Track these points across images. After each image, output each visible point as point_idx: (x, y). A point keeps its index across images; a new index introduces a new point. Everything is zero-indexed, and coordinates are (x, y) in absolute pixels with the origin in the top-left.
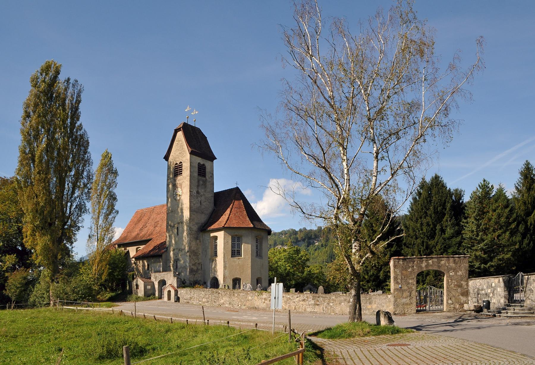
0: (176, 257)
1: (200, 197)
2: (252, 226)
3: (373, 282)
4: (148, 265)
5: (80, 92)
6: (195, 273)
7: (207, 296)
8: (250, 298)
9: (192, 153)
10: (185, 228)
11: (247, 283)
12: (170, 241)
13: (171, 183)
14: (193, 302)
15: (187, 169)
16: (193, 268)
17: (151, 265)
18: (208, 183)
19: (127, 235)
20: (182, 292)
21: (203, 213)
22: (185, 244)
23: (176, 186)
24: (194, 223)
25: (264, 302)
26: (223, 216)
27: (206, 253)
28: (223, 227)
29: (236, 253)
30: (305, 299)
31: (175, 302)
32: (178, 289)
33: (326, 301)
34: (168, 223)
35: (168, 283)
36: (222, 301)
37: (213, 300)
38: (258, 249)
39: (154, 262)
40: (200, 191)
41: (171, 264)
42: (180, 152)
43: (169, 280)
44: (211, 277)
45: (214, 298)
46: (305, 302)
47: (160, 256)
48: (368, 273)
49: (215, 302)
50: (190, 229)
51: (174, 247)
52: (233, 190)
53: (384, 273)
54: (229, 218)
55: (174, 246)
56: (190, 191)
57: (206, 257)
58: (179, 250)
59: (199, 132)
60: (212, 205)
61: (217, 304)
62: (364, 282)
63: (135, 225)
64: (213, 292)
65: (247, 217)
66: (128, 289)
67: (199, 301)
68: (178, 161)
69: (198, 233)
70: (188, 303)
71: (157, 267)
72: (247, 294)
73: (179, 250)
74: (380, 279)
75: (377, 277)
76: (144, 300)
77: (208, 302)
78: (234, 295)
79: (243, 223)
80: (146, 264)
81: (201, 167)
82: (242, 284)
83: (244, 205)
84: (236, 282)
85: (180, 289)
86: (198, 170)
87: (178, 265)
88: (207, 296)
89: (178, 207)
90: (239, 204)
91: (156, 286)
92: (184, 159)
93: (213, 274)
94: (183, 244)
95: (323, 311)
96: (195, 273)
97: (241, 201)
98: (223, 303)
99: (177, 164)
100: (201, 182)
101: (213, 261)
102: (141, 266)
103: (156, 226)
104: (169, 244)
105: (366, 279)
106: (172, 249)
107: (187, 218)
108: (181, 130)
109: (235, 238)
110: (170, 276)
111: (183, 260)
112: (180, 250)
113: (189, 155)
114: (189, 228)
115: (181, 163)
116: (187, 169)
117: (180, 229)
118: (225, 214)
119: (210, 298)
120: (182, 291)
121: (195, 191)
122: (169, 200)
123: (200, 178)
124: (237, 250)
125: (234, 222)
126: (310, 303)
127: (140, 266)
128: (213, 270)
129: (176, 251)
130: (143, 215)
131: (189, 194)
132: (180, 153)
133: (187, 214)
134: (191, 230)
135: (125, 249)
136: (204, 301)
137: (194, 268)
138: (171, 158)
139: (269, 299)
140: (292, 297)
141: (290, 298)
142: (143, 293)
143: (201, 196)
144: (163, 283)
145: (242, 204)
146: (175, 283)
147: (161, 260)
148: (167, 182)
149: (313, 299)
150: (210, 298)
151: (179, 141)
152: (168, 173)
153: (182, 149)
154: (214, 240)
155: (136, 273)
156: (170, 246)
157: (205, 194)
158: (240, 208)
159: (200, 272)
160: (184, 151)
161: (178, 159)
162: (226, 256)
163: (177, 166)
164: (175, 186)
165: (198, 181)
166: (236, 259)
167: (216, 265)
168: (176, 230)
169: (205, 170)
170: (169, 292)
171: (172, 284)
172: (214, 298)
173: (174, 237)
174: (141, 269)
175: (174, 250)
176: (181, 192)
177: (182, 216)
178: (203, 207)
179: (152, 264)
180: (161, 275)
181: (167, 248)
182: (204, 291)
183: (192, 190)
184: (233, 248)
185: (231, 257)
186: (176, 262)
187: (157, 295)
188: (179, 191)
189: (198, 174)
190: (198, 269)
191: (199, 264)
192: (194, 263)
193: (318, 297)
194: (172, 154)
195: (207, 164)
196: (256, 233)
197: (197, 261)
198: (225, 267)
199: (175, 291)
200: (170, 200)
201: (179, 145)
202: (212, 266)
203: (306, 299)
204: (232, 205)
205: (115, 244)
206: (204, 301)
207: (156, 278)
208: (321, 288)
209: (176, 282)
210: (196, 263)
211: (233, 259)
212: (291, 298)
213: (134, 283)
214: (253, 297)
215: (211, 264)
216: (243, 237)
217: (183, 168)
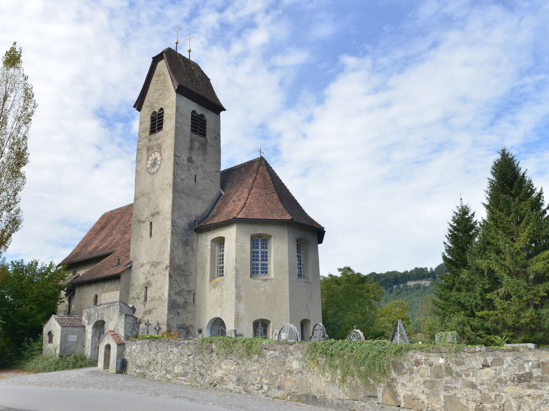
1: (193, 169)
7: (185, 359)
8: (295, 365)
14: (153, 373)
16: (176, 300)
17: (101, 296)
18: (209, 149)
19: (81, 251)
21: (199, 197)
24: (182, 214)
29: (260, 270)
31: (118, 372)
32: (126, 342)
35: (110, 326)
36: (219, 374)
37: (198, 369)
38: (301, 264)
40: (194, 158)
42: (161, 92)
45: (200, 363)
46: (534, 387)
47: (116, 278)
49: (201, 375)
52: (254, 162)
54: (245, 203)
56: (175, 155)
59: (197, 69)
61: (207, 380)
63: (96, 235)
67: (167, 371)
68: (157, 107)
69: (189, 233)
72: (286, 353)
77: (185, 374)
81: (197, 118)
82: (273, 332)
85: (129, 342)
86: (192, 123)
88: (185, 359)
92: (166, 102)
98: (222, 380)
100: (197, 144)
108: (163, 58)
109: (258, 240)
113: (175, 94)
119: (191, 364)
120: (134, 347)
121: (185, 157)
123: (195, 136)
124: (258, 260)
130: (110, 219)
131: (172, 160)
132: (160, 95)
135: (74, 274)
136: (176, 371)
137: (178, 299)
143: (197, 168)
146: (121, 327)
153: (165, 87)
157: (203, 164)
161: (156, 105)
165: (192, 141)
166: (258, 281)
169: (205, 125)
171: (116, 331)
172: (200, 363)
182: (177, 346)
183: (177, 154)
184: (253, 260)
185: (251, 277)
189: (192, 130)
190: (186, 302)
192: (179, 290)
194: (148, 98)
195: (209, 116)
201: (160, 82)
206: (176, 371)
210: (182, 290)
216: (272, 238)
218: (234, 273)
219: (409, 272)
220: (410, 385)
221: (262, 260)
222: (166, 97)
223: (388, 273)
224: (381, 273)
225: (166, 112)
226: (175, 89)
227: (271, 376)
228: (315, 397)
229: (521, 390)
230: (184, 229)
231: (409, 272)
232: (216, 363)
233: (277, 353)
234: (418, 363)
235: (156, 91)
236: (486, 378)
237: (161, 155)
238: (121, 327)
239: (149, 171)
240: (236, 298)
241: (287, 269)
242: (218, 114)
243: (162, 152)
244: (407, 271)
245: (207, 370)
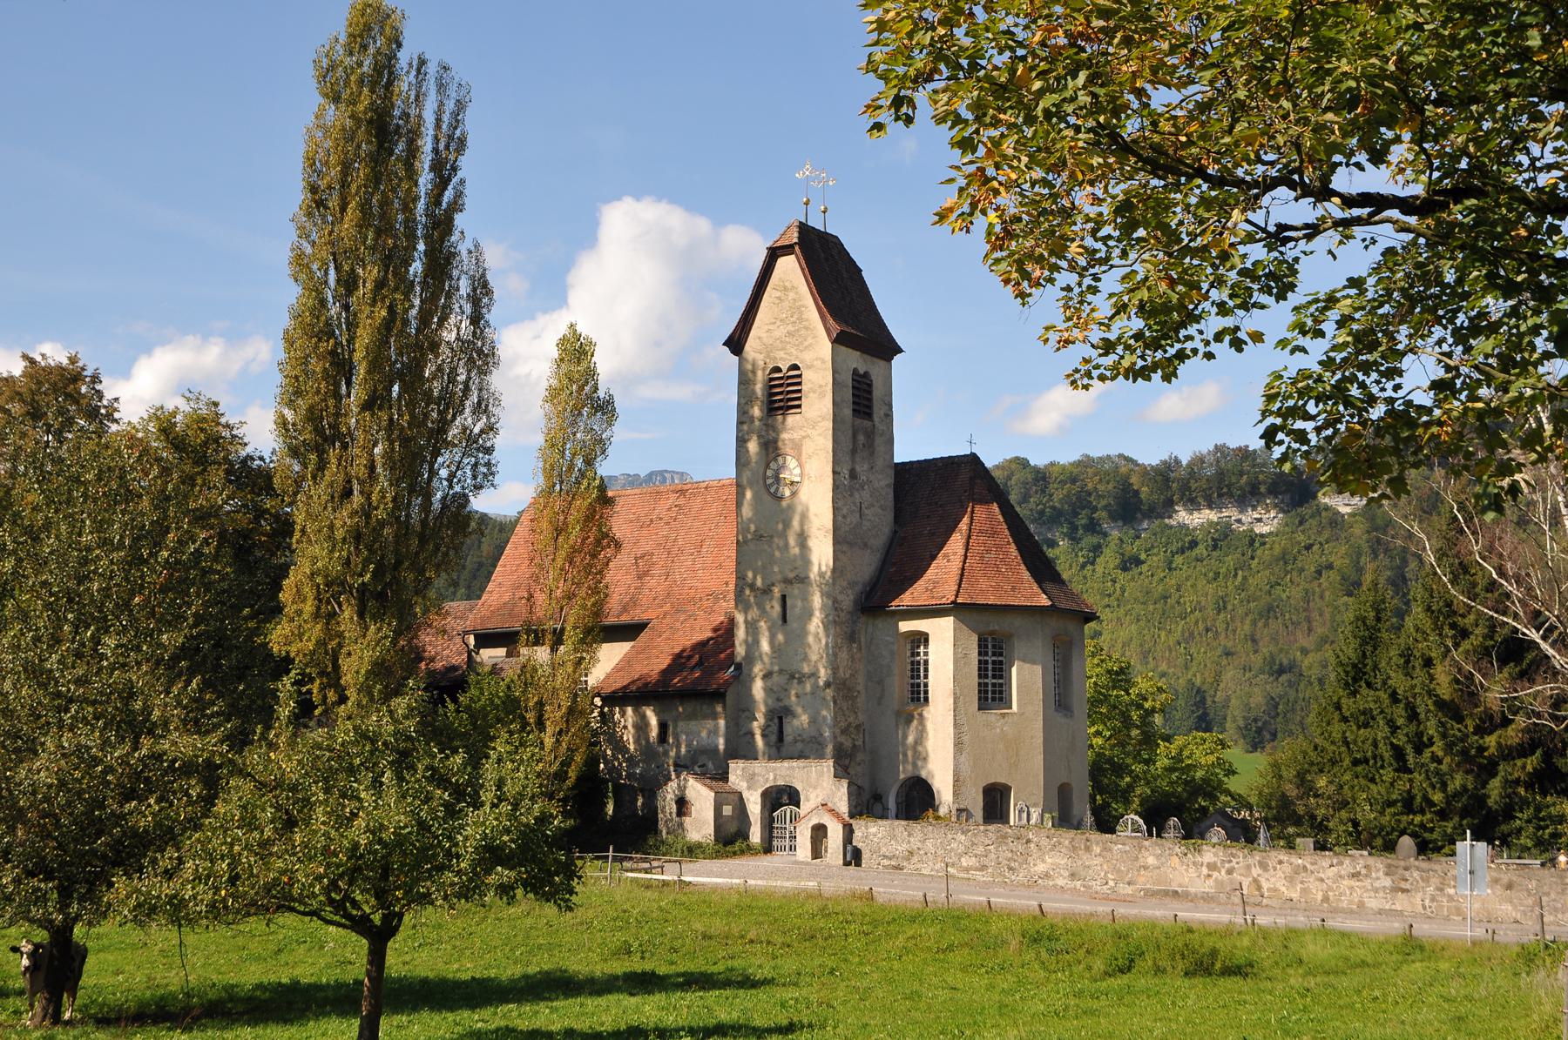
0: (779, 700)
2: (1044, 601)
3: (1462, 818)
4: (663, 727)
5: (461, 106)
6: (847, 762)
8: (1151, 860)
9: (839, 340)
10: (817, 601)
11: (1027, 805)
12: (752, 645)
13: (755, 438)
15: (823, 395)
17: (675, 727)
20: (871, 833)
22: (814, 657)
23: (777, 448)
24: (845, 584)
25: (1209, 876)
26: (939, 561)
27: (883, 690)
28: (952, 603)
30: (1359, 873)
32: (851, 821)
33: (1433, 880)
34: (741, 578)
36: (1041, 868)
39: (691, 717)
40: (858, 468)
41: (757, 727)
42: (790, 328)
43: (815, 788)
44: (902, 776)
45: (1010, 855)
47: (718, 696)
48: (1444, 785)
49: (1010, 869)
50: (834, 605)
51: (768, 666)
53: (1504, 788)
54: (963, 569)
55: (766, 659)
56: (834, 472)
57: (879, 703)
58: (787, 674)
60: (890, 516)
62: (1429, 816)
64: (1005, 837)
65: (1023, 567)
66: (610, 812)
68: (781, 359)
70: (898, 868)
71: (704, 734)
73: (792, 677)
74: (1490, 808)
75: (1481, 800)
76: (718, 855)
77: (983, 868)
78: (1088, 849)
79: (1013, 589)
80: (653, 721)
83: (1006, 522)
84: (995, 803)
85: (862, 822)
87: (787, 730)
89: (787, 524)
90: (991, 518)
91: (754, 807)
93: (910, 768)
94: (806, 658)
95: (1424, 908)
96: (847, 762)
97: (995, 507)
99: (778, 370)
100: (861, 438)
101: (909, 721)
102: (630, 728)
103: (646, 573)
104: (747, 652)
105: (1435, 805)
106: (758, 669)
107: (824, 568)
110: (820, 775)
111: (805, 710)
112: (795, 677)
113: (829, 345)
114: (830, 602)
115: (795, 367)
116: (823, 395)
117: (795, 605)
118: (946, 556)
119: (993, 856)
122: (744, 495)
123: (858, 421)
125: (984, 584)
126: (1377, 884)
127: (625, 727)
128: (910, 753)
129: (775, 678)
131: (829, 481)
132: (790, 334)
133: (822, 553)
134: (836, 609)
136: (965, 864)
138: (752, 346)
139: (1227, 865)
140: (1312, 864)
141: (1305, 867)
142: (711, 830)
144: (781, 798)
145: (1000, 517)
146: (841, 800)
147: (719, 709)
148: (738, 430)
149: (1387, 874)
150: (993, 856)
151: (785, 289)
152: (743, 401)
154: (909, 647)
155: (609, 752)
156: (750, 658)
158: (994, 534)
159: (860, 757)
160: (807, 328)
161: (781, 354)
162: (960, 704)
163: (781, 378)
164: (771, 449)
167: (922, 732)
168: (778, 608)
170: (819, 832)
172: (1010, 855)
173: (770, 629)
174: (629, 737)
175: (767, 676)
176: (797, 471)
177: (807, 562)
178: (866, 525)
179: (681, 724)
180: (774, 770)
181: (739, 667)
186: (776, 721)
187: (756, 836)
188: (792, 471)
189: (854, 410)
190: (854, 746)
191: (858, 727)
193: (1406, 869)
195: (874, 368)
196: (1055, 624)
197: (851, 719)
198: (958, 745)
199: (844, 826)
200: (749, 495)
201: (786, 304)
202: (905, 737)
203: (1364, 871)
204: (966, 519)
205: (467, 633)
207: (751, 779)
208: (1406, 842)
209: (845, 798)
211: (985, 716)
212: (1309, 866)
213: (670, 792)
214: (1163, 860)
215: (900, 733)
217: (804, 387)
218: (952, 701)
219: (1184, 463)
220: (1273, 880)
221: (994, 677)
222: (806, 343)
223: (1086, 463)
224: (1052, 464)
225: (808, 376)
226: (829, 335)
227: (1119, 871)
228: (1177, 892)
229: (1352, 883)
230: (849, 612)
231: (1184, 463)
232: (1035, 856)
233: (1127, 848)
234: (1280, 862)
235: (778, 323)
236: (1331, 874)
237: (800, 465)
238: (841, 800)
239: (772, 490)
240: (955, 745)
241: (1041, 696)
242: (889, 359)
243: (804, 456)
244: (1177, 461)
245: (1021, 864)
